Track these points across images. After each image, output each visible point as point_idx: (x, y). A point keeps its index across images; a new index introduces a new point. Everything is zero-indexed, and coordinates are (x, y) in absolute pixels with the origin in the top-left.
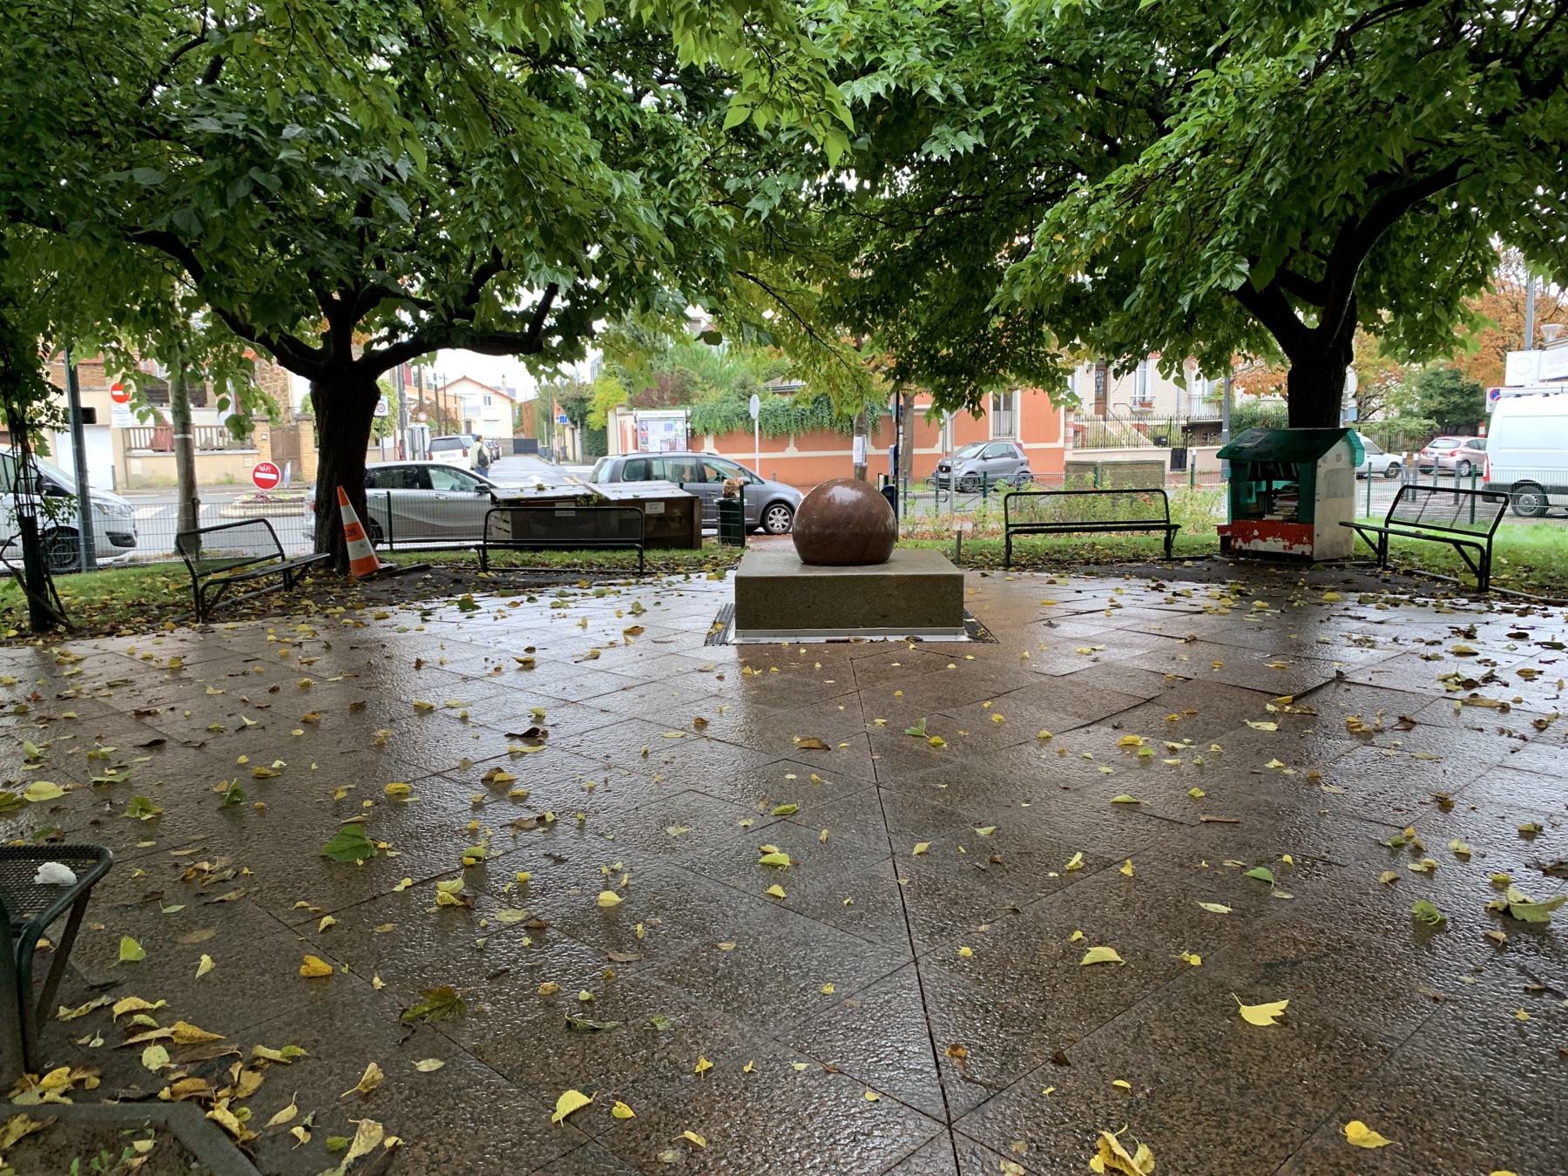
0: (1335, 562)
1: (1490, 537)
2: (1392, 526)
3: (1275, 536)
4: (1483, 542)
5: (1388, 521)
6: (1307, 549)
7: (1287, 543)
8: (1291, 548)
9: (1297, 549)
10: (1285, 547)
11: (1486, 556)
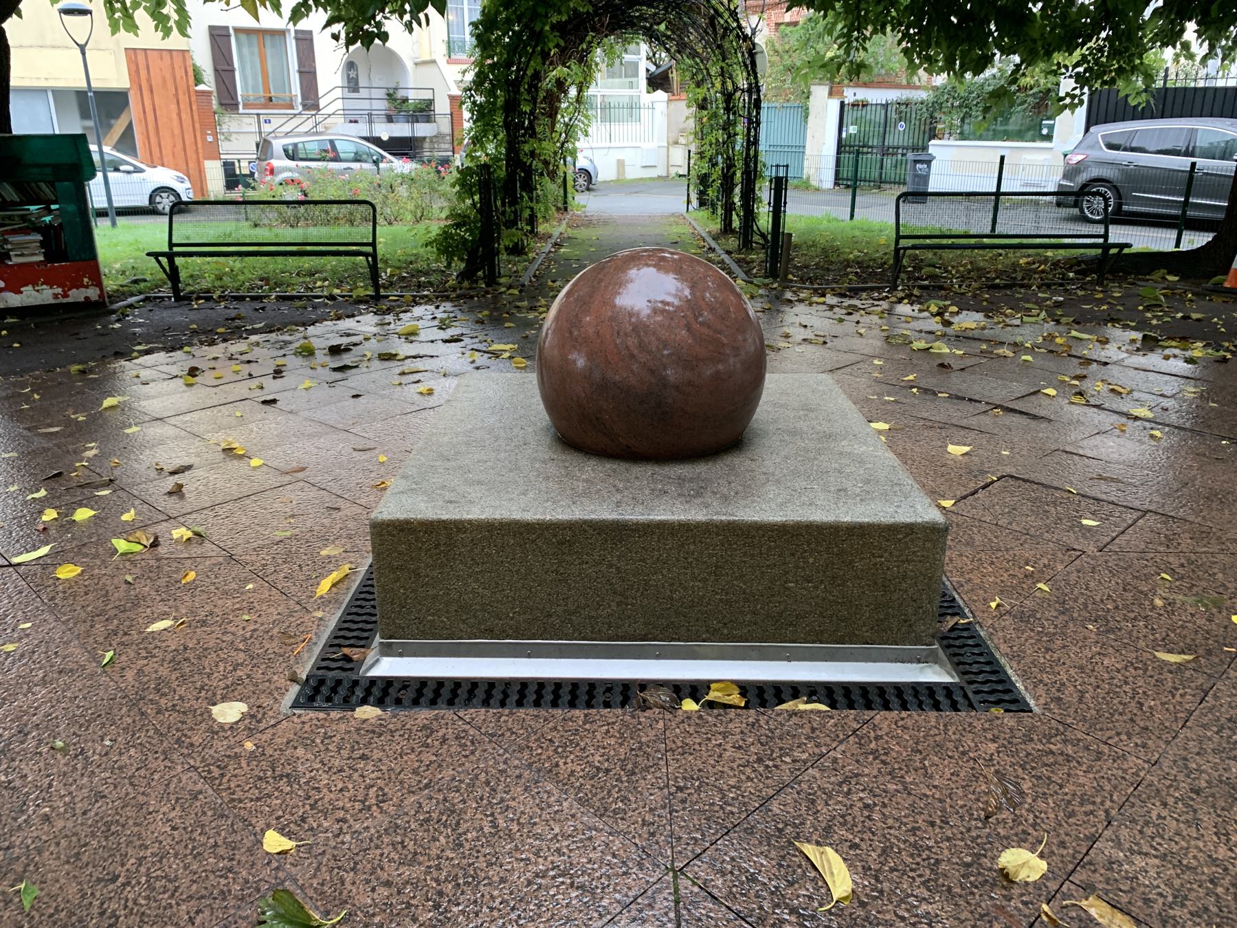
0: (120, 294)
1: (373, 244)
2: (176, 249)
3: (34, 284)
4: (369, 249)
5: (171, 245)
6: (93, 293)
7: (60, 290)
8: (65, 295)
9: (77, 295)
10: (56, 296)
11: (374, 255)
